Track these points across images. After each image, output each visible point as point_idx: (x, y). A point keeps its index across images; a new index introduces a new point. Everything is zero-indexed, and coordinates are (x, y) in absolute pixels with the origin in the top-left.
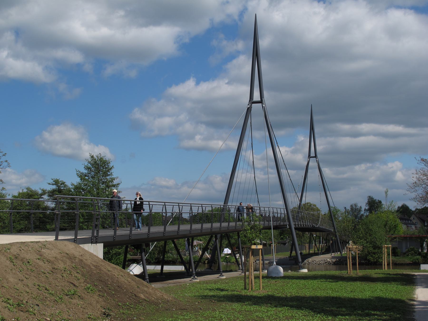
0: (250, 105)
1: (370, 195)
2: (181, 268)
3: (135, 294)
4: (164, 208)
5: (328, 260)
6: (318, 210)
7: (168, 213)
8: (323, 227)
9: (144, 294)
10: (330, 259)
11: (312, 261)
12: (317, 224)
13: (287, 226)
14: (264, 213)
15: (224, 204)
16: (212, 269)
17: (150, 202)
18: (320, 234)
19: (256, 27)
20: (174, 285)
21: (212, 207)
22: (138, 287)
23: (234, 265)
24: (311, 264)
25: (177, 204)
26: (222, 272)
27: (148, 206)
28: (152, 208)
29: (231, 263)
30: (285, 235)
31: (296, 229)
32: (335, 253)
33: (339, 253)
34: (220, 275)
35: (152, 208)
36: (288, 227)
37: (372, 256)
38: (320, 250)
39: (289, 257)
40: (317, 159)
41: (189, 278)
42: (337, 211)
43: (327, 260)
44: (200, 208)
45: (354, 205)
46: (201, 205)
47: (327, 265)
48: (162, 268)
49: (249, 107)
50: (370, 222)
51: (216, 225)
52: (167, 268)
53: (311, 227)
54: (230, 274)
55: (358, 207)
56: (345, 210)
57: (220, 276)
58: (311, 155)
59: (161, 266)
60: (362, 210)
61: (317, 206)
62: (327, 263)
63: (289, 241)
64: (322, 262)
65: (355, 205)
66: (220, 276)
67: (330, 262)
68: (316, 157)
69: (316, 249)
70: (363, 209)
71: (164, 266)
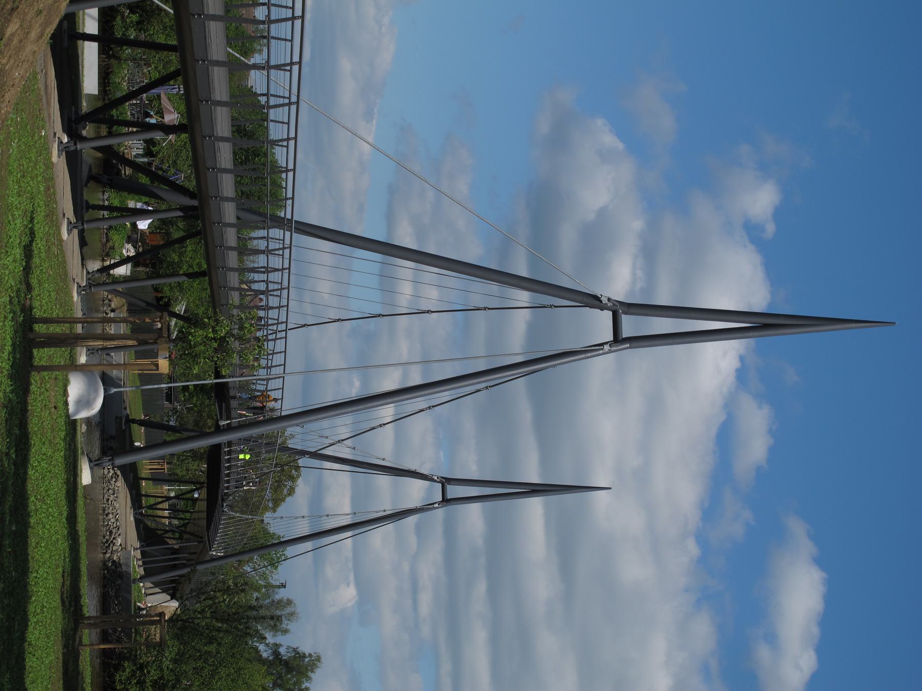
0: (610, 304)
1: (323, 660)
2: (90, 83)
3: (18, 8)
4: (281, 101)
5: (119, 540)
6: (277, 502)
7: (268, 231)
8: (217, 541)
9: (19, 31)
10: (121, 545)
11: (116, 489)
12: (231, 507)
13: (227, 420)
14: (268, 102)
15: (295, 221)
16: (87, 182)
17: (300, 20)
18: (202, 512)
19: (854, 325)
20: (43, 89)
21: (287, 171)
22: (39, 12)
23: (101, 241)
24: (105, 485)
25: (292, 135)
26: (81, 228)
27: (288, 61)
28: (277, 255)
29: (106, 234)
30: (197, 396)
31: (217, 448)
32: (139, 560)
33: (141, 571)
34: (73, 220)
35: (277, 255)
36: (223, 423)
37: (133, 674)
38: (150, 512)
39: (128, 416)
40: (436, 505)
41: (61, 124)
42: (274, 564)
43: (119, 535)
44: (276, 286)
45: (293, 609)
46: (298, 60)
47: (104, 537)
48: (90, 38)
49: (601, 302)
50: (240, 669)
51: (227, 185)
52: (90, 53)
53: (223, 490)
54: (75, 262)
55: (287, 625)
56: (278, 584)
57: (68, 221)
58: (449, 488)
59: (96, 33)
60: (276, 636)
61: (288, 499)
62: (108, 538)
63: (177, 412)
64: (113, 520)
65: (292, 614)
66: (69, 223)
67: (111, 545)
68: (445, 503)
69: (152, 501)
70: (280, 639)
71: (97, 43)
